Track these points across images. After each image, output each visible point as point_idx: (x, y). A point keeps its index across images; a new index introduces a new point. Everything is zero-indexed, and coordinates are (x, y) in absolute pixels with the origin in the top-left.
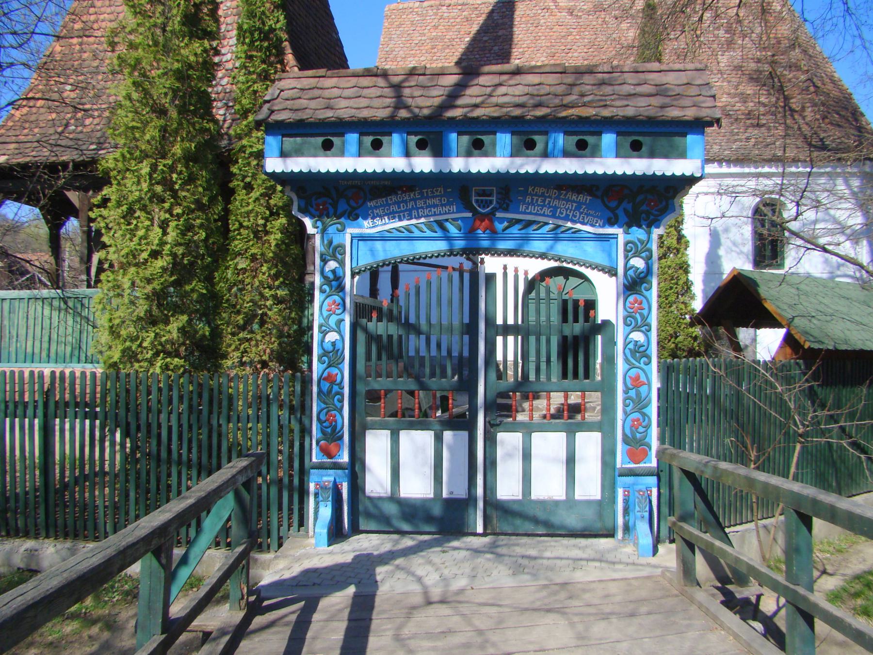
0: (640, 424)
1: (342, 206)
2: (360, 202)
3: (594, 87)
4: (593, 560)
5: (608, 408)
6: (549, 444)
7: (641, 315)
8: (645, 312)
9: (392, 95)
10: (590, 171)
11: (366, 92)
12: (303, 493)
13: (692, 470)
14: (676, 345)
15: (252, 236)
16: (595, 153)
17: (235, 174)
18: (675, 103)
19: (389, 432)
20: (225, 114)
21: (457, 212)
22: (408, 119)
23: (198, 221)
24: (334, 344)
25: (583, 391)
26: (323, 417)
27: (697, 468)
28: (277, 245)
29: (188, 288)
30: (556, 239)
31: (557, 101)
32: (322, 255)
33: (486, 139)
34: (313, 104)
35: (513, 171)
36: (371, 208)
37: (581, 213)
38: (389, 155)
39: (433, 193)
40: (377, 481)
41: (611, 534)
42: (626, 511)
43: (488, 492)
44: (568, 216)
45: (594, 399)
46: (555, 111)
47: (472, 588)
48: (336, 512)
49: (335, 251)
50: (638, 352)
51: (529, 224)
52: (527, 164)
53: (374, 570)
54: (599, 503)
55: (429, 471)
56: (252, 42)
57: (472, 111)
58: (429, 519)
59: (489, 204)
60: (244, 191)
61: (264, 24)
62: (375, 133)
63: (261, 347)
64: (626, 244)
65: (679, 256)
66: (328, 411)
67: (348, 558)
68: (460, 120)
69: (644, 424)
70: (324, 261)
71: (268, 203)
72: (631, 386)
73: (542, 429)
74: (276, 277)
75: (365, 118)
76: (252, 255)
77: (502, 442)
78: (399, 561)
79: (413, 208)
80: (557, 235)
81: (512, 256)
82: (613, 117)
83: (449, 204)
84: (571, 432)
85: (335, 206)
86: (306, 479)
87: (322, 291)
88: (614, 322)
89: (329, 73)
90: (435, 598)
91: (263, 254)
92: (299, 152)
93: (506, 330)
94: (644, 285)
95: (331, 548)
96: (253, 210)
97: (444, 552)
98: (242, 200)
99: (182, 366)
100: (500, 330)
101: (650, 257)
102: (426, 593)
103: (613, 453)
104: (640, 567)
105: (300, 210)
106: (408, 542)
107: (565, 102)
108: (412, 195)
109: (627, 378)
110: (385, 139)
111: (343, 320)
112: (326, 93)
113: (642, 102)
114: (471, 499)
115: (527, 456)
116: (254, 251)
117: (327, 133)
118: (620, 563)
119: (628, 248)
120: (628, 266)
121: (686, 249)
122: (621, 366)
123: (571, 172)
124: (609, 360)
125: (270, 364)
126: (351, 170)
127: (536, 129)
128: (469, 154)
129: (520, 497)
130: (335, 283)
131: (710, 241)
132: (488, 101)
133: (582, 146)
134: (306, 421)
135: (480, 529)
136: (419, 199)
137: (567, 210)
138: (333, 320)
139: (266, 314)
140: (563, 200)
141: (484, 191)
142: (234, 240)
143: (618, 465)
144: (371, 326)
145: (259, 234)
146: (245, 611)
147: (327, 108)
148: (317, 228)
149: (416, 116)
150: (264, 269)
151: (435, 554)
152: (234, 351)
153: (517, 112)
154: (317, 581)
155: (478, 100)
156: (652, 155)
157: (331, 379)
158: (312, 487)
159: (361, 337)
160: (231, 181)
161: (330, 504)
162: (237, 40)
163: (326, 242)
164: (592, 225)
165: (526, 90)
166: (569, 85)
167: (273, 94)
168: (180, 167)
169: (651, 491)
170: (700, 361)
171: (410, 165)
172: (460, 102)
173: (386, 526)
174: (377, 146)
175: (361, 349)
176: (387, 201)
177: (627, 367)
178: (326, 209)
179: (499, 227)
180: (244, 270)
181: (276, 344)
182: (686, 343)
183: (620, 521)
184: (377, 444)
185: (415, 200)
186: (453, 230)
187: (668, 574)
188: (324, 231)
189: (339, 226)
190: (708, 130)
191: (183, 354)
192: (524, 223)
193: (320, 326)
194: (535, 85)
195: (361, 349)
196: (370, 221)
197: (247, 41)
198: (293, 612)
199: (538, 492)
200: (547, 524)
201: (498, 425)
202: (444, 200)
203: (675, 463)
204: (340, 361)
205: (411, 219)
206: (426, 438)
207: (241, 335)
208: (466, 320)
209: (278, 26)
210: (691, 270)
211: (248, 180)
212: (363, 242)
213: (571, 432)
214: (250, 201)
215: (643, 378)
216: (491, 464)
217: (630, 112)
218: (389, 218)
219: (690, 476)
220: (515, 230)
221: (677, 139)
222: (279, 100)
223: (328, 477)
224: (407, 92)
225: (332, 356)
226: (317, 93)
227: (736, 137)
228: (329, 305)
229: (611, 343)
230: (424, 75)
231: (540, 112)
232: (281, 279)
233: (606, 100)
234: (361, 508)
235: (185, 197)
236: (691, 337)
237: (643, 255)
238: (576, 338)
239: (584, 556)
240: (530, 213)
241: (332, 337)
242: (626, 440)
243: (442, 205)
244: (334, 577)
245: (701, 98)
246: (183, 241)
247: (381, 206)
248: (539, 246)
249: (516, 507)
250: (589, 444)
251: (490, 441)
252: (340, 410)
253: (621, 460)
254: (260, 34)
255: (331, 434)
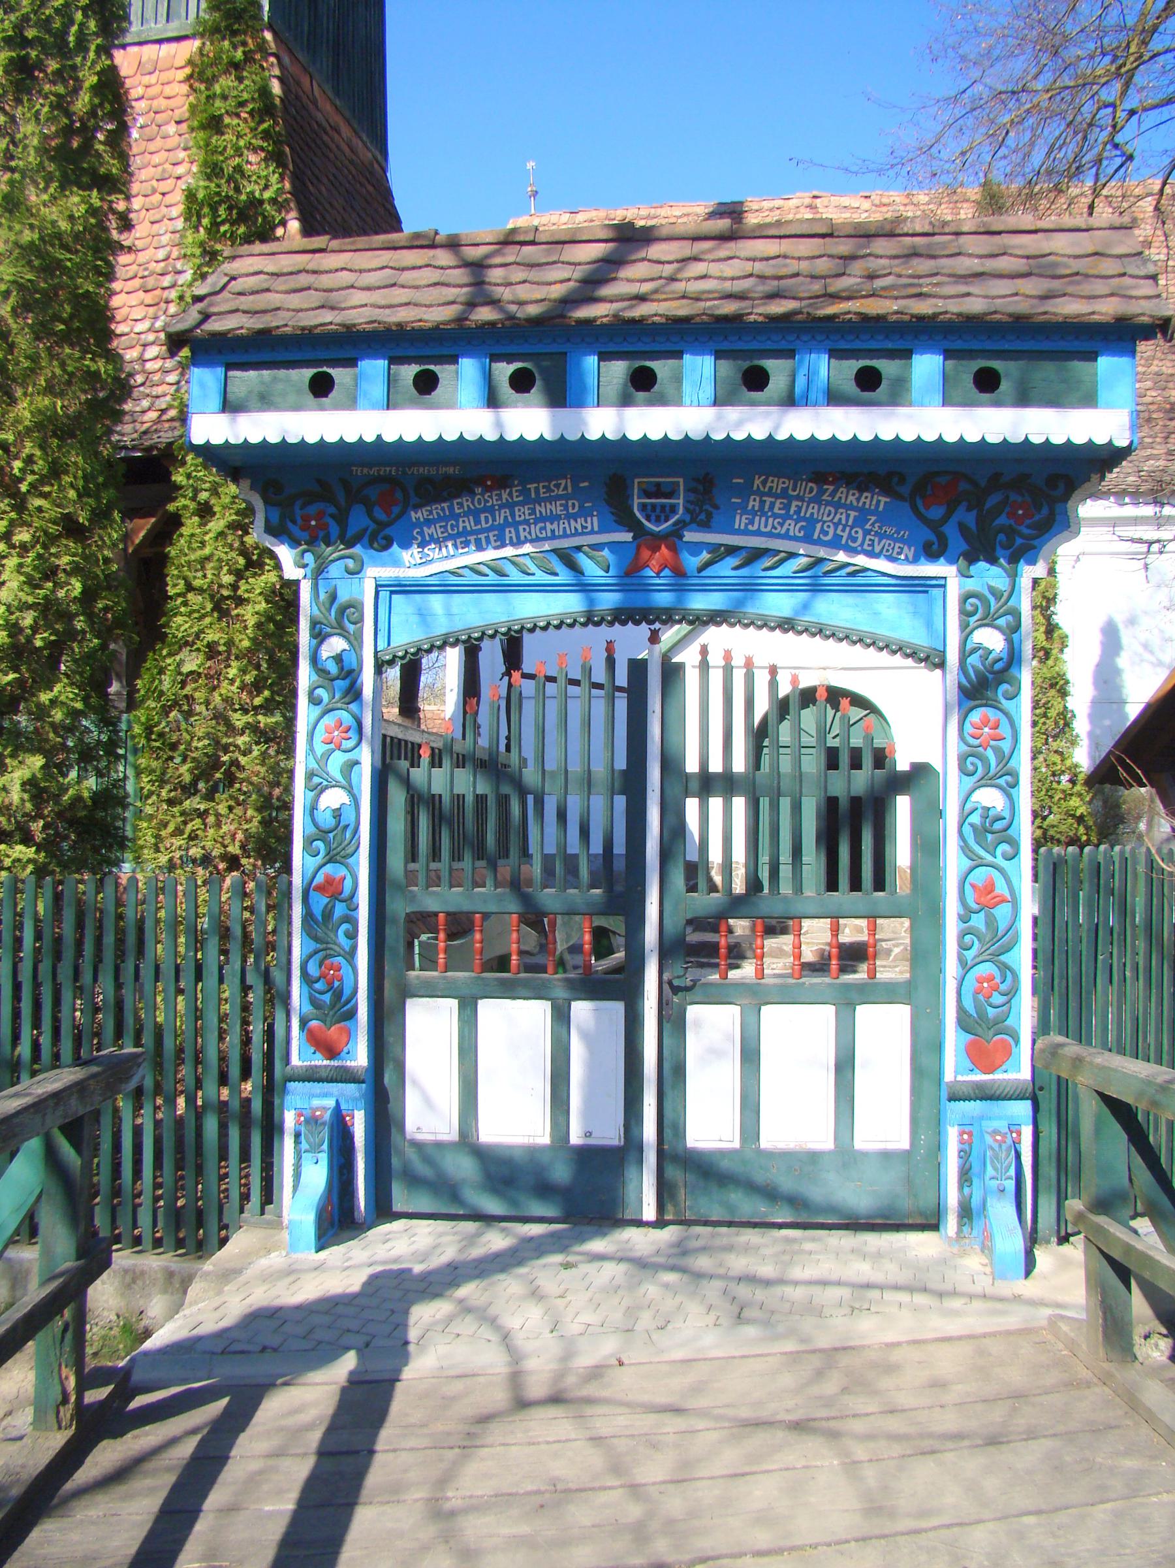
0: (996, 989)
1: (358, 519)
2: (396, 510)
3: (896, 262)
4: (896, 1288)
5: (925, 955)
6: (798, 1034)
7: (998, 751)
8: (1006, 746)
9: (466, 280)
10: (887, 435)
11: (407, 277)
12: (271, 1129)
13: (1128, 1099)
14: (1045, 831)
15: (209, 606)
16: (898, 396)
17: (181, 487)
18: (1070, 289)
19: (454, 1003)
20: (178, 383)
21: (599, 532)
22: (493, 324)
23: (66, 559)
24: (337, 813)
25: (872, 917)
26: (313, 970)
27: (1140, 1095)
28: (259, 626)
29: (45, 697)
30: (816, 588)
31: (817, 287)
32: (314, 623)
33: (661, 367)
34: (295, 301)
35: (718, 436)
36: (418, 524)
37: (867, 533)
38: (451, 405)
39: (549, 490)
40: (428, 1113)
41: (931, 1223)
42: (965, 1176)
43: (668, 1132)
44: (838, 537)
45: (896, 933)
46: (810, 305)
47: (621, 1364)
48: (341, 1174)
49: (343, 617)
50: (991, 832)
51: (756, 555)
52: (749, 420)
53: (406, 1312)
54: (906, 1155)
55: (541, 1087)
56: (215, 225)
57: (631, 307)
58: (544, 1189)
59: (661, 507)
60: (196, 519)
61: (237, 190)
62: (420, 354)
63: (225, 828)
64: (965, 598)
65: (1050, 662)
66: (327, 957)
67: (353, 1283)
68: (603, 325)
69: (1003, 987)
70: (320, 636)
71: (242, 543)
72: (974, 906)
73: (787, 996)
74: (257, 687)
75: (399, 325)
76: (209, 645)
77: (698, 1024)
78: (466, 1291)
79: (507, 524)
80: (816, 580)
81: (719, 624)
82: (935, 315)
83: (584, 513)
84: (847, 1002)
85: (342, 520)
86: (277, 1101)
87: (314, 701)
88: (937, 765)
89: (335, 244)
90: (536, 1388)
91: (230, 643)
92: (266, 401)
93: (707, 784)
94: (1004, 687)
95: (323, 1254)
96: (212, 555)
97: (567, 1266)
98: (192, 535)
99: (30, 861)
100: (694, 785)
101: (1016, 627)
102: (516, 1378)
103: (938, 1047)
104: (999, 1306)
105: (270, 530)
106: (496, 1240)
107: (831, 290)
108: (505, 496)
109: (967, 887)
110: (443, 372)
111: (357, 763)
112: (326, 281)
113: (1002, 287)
114: (632, 1145)
115: (750, 1055)
116: (211, 636)
117: (321, 356)
118: (954, 1293)
119: (969, 608)
120: (969, 646)
121: (1061, 651)
122: (953, 862)
123: (844, 437)
124: (928, 847)
125: (244, 861)
126: (370, 438)
127: (769, 345)
128: (625, 401)
129: (736, 1144)
130: (345, 682)
131: (1102, 643)
132: (668, 289)
133: (868, 380)
134: (277, 976)
135: (649, 1212)
136: (522, 503)
137: (836, 525)
138: (337, 762)
139: (235, 763)
140: (828, 504)
141: (658, 485)
142: (175, 615)
143: (949, 1076)
144: (418, 775)
145: (223, 606)
146: (70, 1432)
147: (323, 307)
148: (305, 566)
149: (512, 318)
150: (232, 672)
151: (547, 1272)
152: (173, 834)
153: (729, 308)
154: (274, 1341)
155: (646, 288)
156: (1023, 399)
157: (332, 888)
158: (290, 1119)
159: (397, 797)
160: (174, 499)
161: (324, 1158)
162: (186, 220)
163: (323, 596)
164: (892, 559)
165: (748, 267)
166: (841, 258)
167: (214, 284)
168: (29, 448)
169: (1019, 1133)
170: (1122, 852)
171: (499, 424)
172: (606, 291)
173: (450, 1203)
174: (426, 384)
175: (397, 825)
176: (451, 508)
177: (967, 863)
178: (325, 527)
179: (692, 562)
180: (194, 675)
181: (255, 823)
182: (1063, 828)
183: (952, 1198)
184: (429, 1025)
185: (511, 506)
186: (591, 569)
187: (1065, 1328)
188: (319, 572)
189: (350, 563)
190: (1143, 347)
191: (39, 837)
192: (744, 554)
193: (310, 775)
194: (767, 259)
195: (397, 825)
196: (415, 550)
197: (206, 222)
198: (194, 1431)
199: (775, 1134)
200: (795, 1201)
201: (687, 989)
202: (574, 507)
203: (1084, 1081)
204: (350, 850)
205: (503, 546)
206: (532, 1015)
207: (187, 804)
208: (621, 764)
209: (267, 195)
210: (1070, 688)
211: (203, 496)
212: (411, 597)
213: (847, 1002)
214: (207, 538)
215: (1001, 888)
216: (673, 1074)
217: (975, 306)
218: (455, 546)
219: (1121, 1111)
220: (725, 568)
221: (1078, 366)
222: (225, 294)
223: (322, 1100)
224: (495, 275)
225: (333, 840)
226: (304, 280)
227: (1149, 452)
228: (328, 731)
229: (929, 815)
230: (533, 243)
231: (778, 308)
232: (267, 693)
233: (920, 286)
234: (395, 1162)
235: (40, 509)
236: (1073, 816)
237: (1001, 622)
238: (856, 802)
239: (878, 1277)
240: (758, 533)
241: (333, 798)
242: (964, 1022)
243: (569, 517)
244: (311, 1331)
245: (1126, 281)
246: (30, 600)
247: (440, 519)
248: (778, 604)
249: (725, 1164)
250: (884, 1030)
251: (673, 1023)
252: (351, 954)
253: (954, 1065)
254: (230, 209)
255: (333, 1006)
